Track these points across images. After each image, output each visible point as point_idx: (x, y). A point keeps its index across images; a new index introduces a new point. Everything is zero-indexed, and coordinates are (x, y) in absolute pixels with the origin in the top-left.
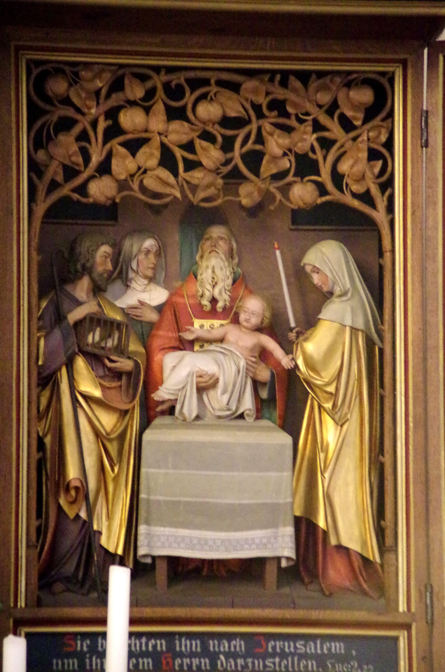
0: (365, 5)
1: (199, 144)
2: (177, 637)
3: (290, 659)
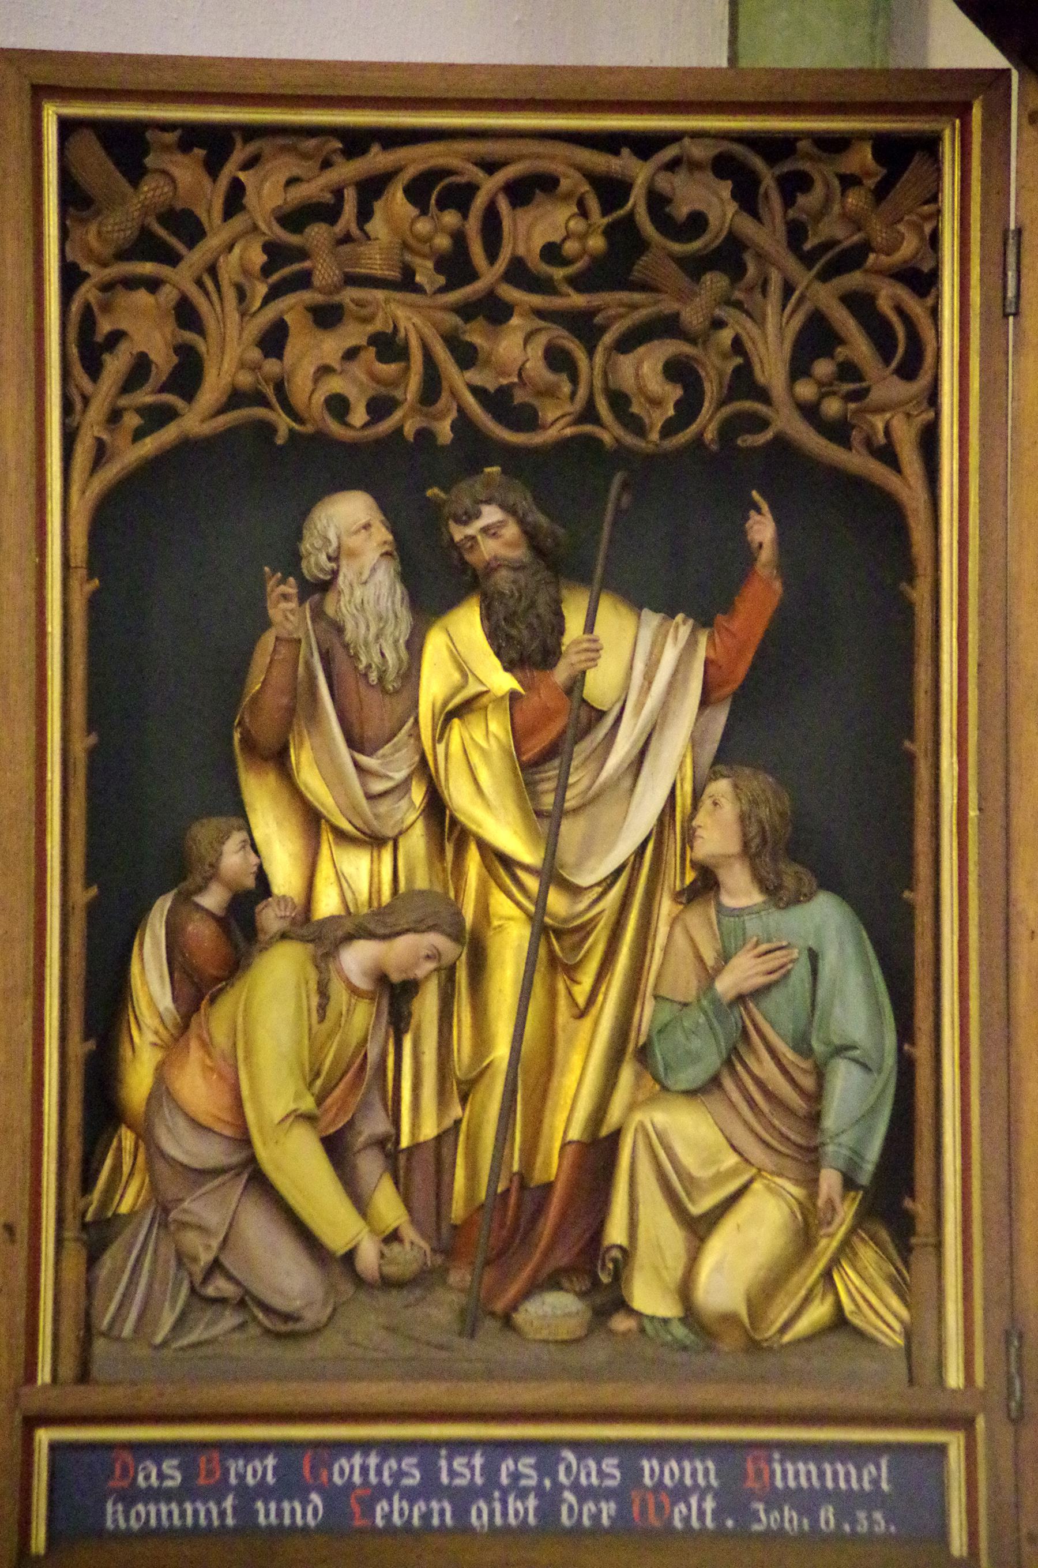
0: (917, 253)
1: (475, 335)
2: (443, 1452)
3: (694, 1501)
